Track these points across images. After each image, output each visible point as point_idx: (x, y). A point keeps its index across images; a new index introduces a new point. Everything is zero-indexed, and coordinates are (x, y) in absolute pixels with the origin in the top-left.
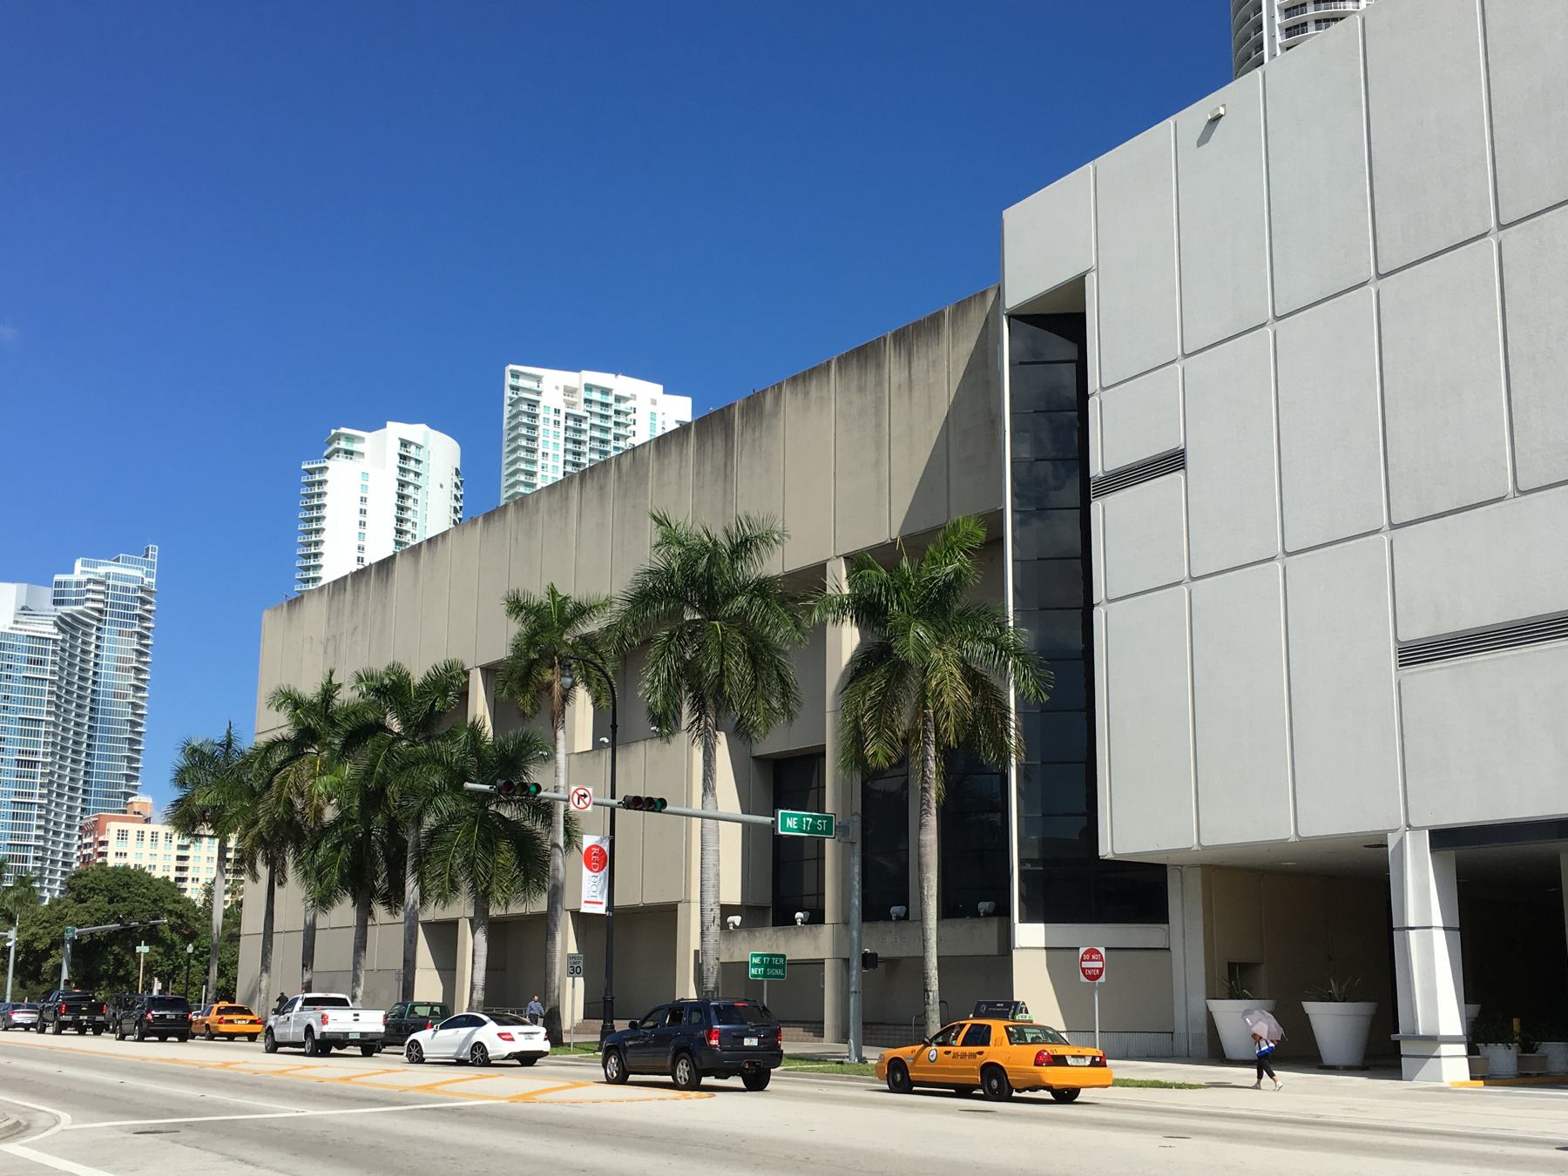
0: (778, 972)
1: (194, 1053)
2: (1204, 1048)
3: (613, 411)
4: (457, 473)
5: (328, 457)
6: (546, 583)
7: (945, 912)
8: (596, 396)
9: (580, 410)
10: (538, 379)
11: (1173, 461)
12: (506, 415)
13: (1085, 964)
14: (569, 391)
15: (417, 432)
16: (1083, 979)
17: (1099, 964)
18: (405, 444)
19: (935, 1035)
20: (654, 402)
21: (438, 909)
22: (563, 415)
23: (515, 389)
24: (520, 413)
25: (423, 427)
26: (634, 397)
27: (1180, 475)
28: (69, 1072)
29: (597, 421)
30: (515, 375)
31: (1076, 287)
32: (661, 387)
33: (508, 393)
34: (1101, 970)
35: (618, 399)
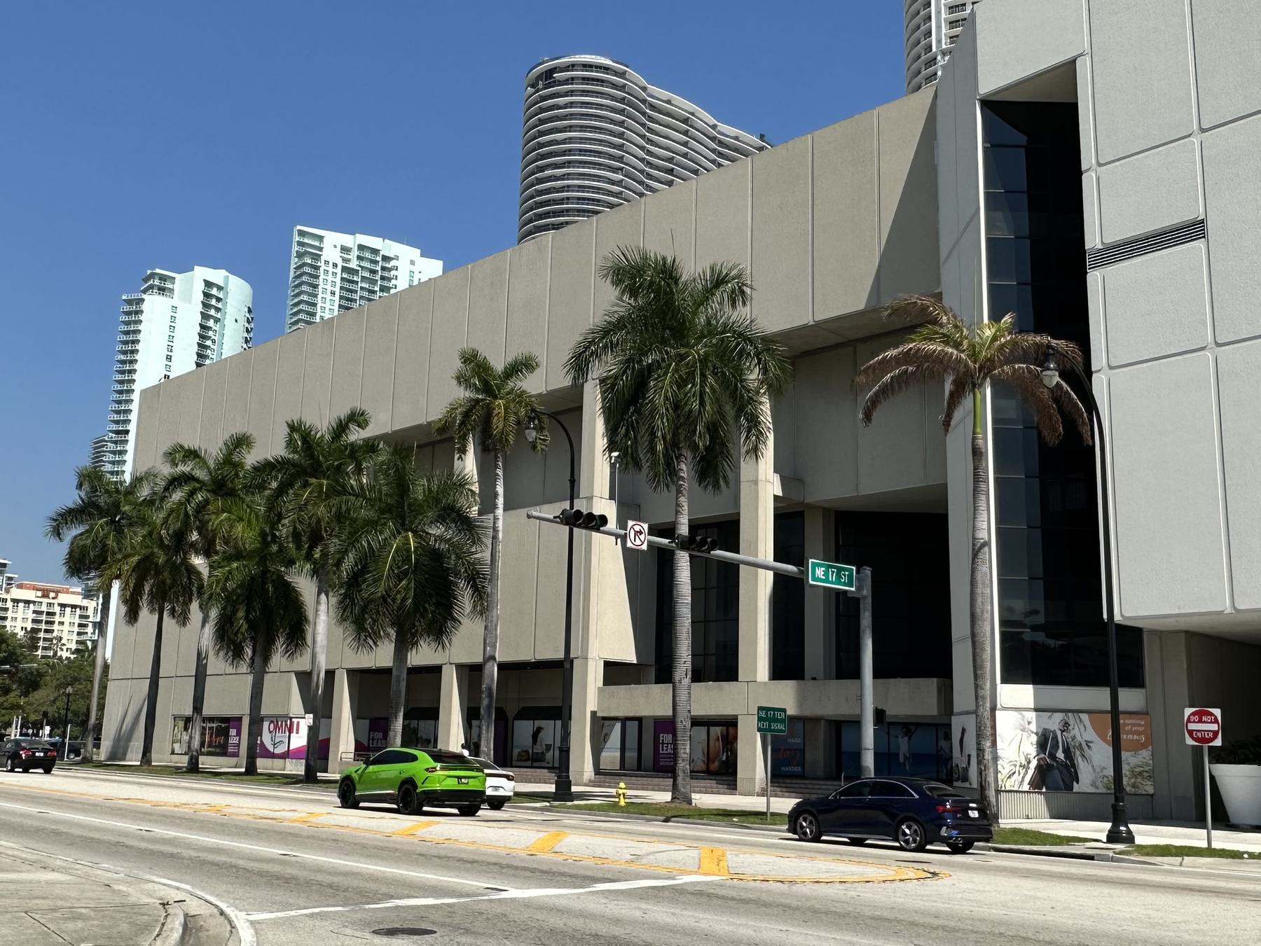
0: (780, 727)
1: (62, 782)
2: (1193, 813)
3: (379, 269)
4: (250, 311)
5: (145, 291)
6: (238, 428)
7: (876, 675)
8: (368, 255)
9: (353, 265)
10: (321, 238)
11: (1194, 230)
12: (293, 266)
13: (1192, 726)
14: (345, 250)
15: (217, 276)
16: (1190, 742)
17: (1214, 727)
18: (208, 284)
19: (897, 790)
20: (412, 263)
21: (284, 660)
22: (339, 268)
23: (300, 244)
24: (305, 264)
25: (223, 273)
26: (397, 258)
27: (1200, 244)
28: (54, 813)
29: (367, 274)
30: (301, 233)
31: (1068, 70)
32: (418, 251)
33: (295, 248)
34: (1215, 734)
35: (385, 259)
